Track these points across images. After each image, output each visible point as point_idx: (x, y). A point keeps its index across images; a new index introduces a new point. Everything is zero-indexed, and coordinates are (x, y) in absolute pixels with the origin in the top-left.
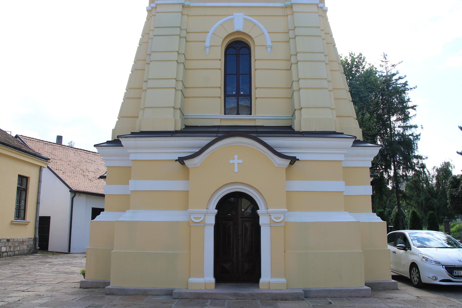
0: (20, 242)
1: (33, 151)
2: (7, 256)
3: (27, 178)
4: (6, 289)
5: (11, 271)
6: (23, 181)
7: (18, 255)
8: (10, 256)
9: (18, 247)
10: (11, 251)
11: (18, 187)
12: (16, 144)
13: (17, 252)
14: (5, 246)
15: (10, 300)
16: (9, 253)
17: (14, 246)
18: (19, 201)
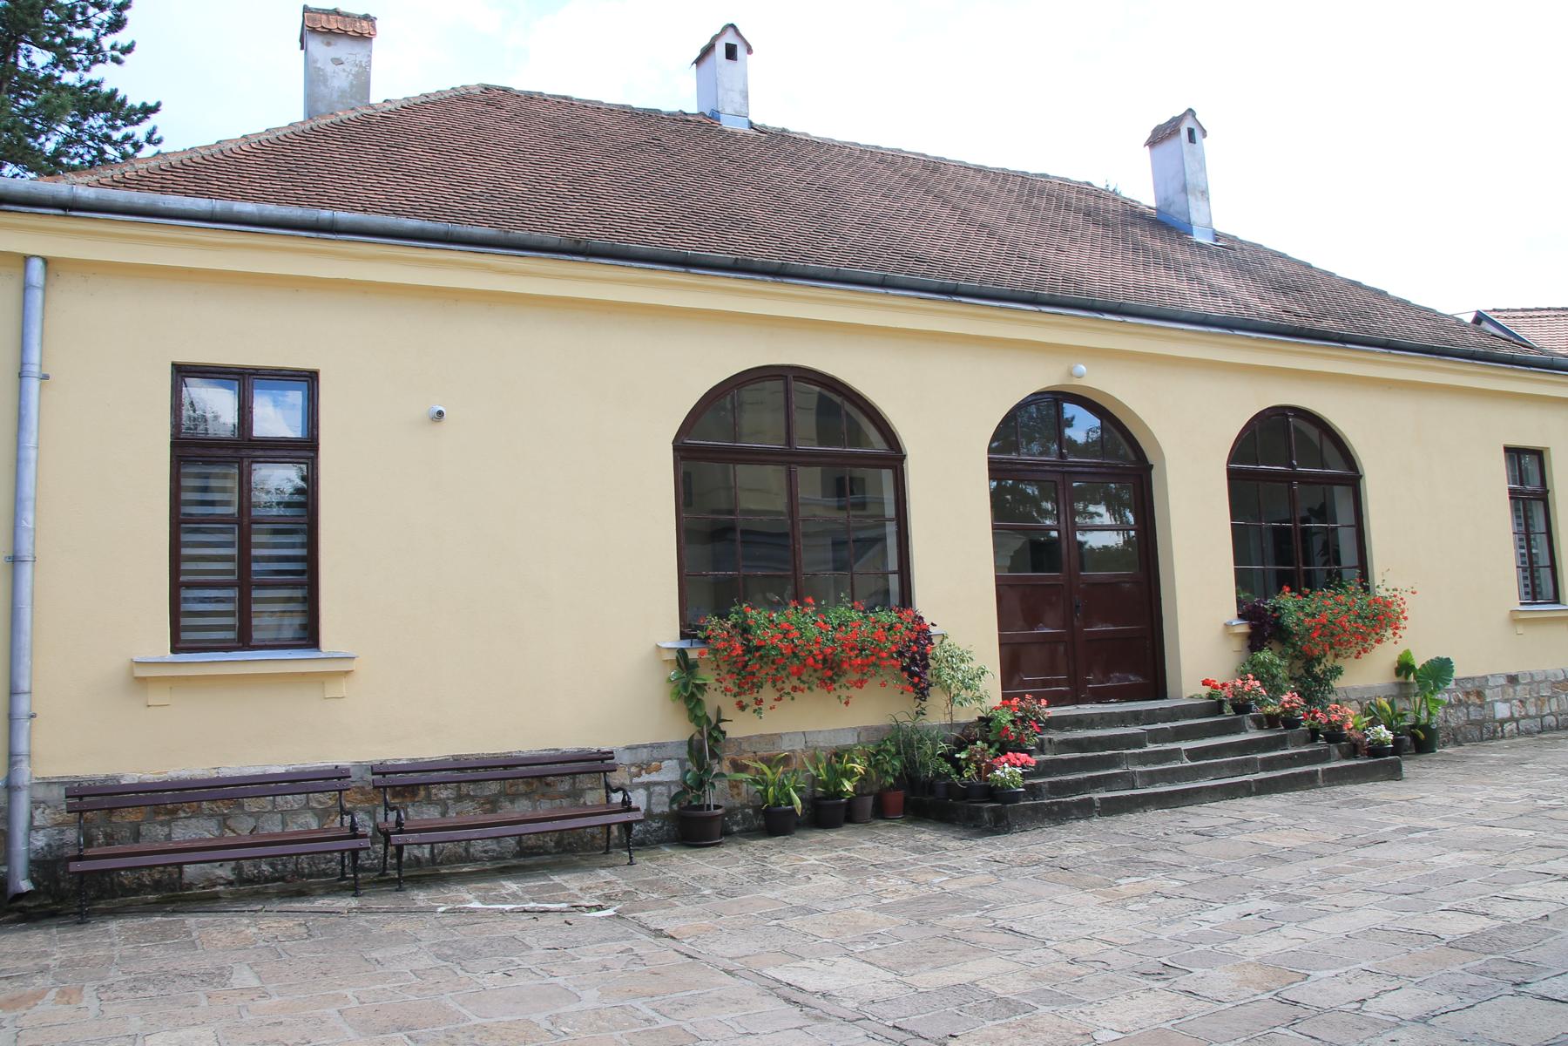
0: (1555, 684)
1: (1542, 352)
2: (1520, 733)
3: (1539, 454)
4: (1501, 865)
5: (1527, 791)
6: (1528, 472)
7: (1558, 728)
8: (1529, 733)
9: (1554, 701)
10: (1527, 716)
11: (1512, 492)
12: (1473, 341)
13: (1550, 720)
14: (1506, 701)
15: (1510, 911)
16: (1522, 722)
17: (1538, 699)
18: (1525, 536)
